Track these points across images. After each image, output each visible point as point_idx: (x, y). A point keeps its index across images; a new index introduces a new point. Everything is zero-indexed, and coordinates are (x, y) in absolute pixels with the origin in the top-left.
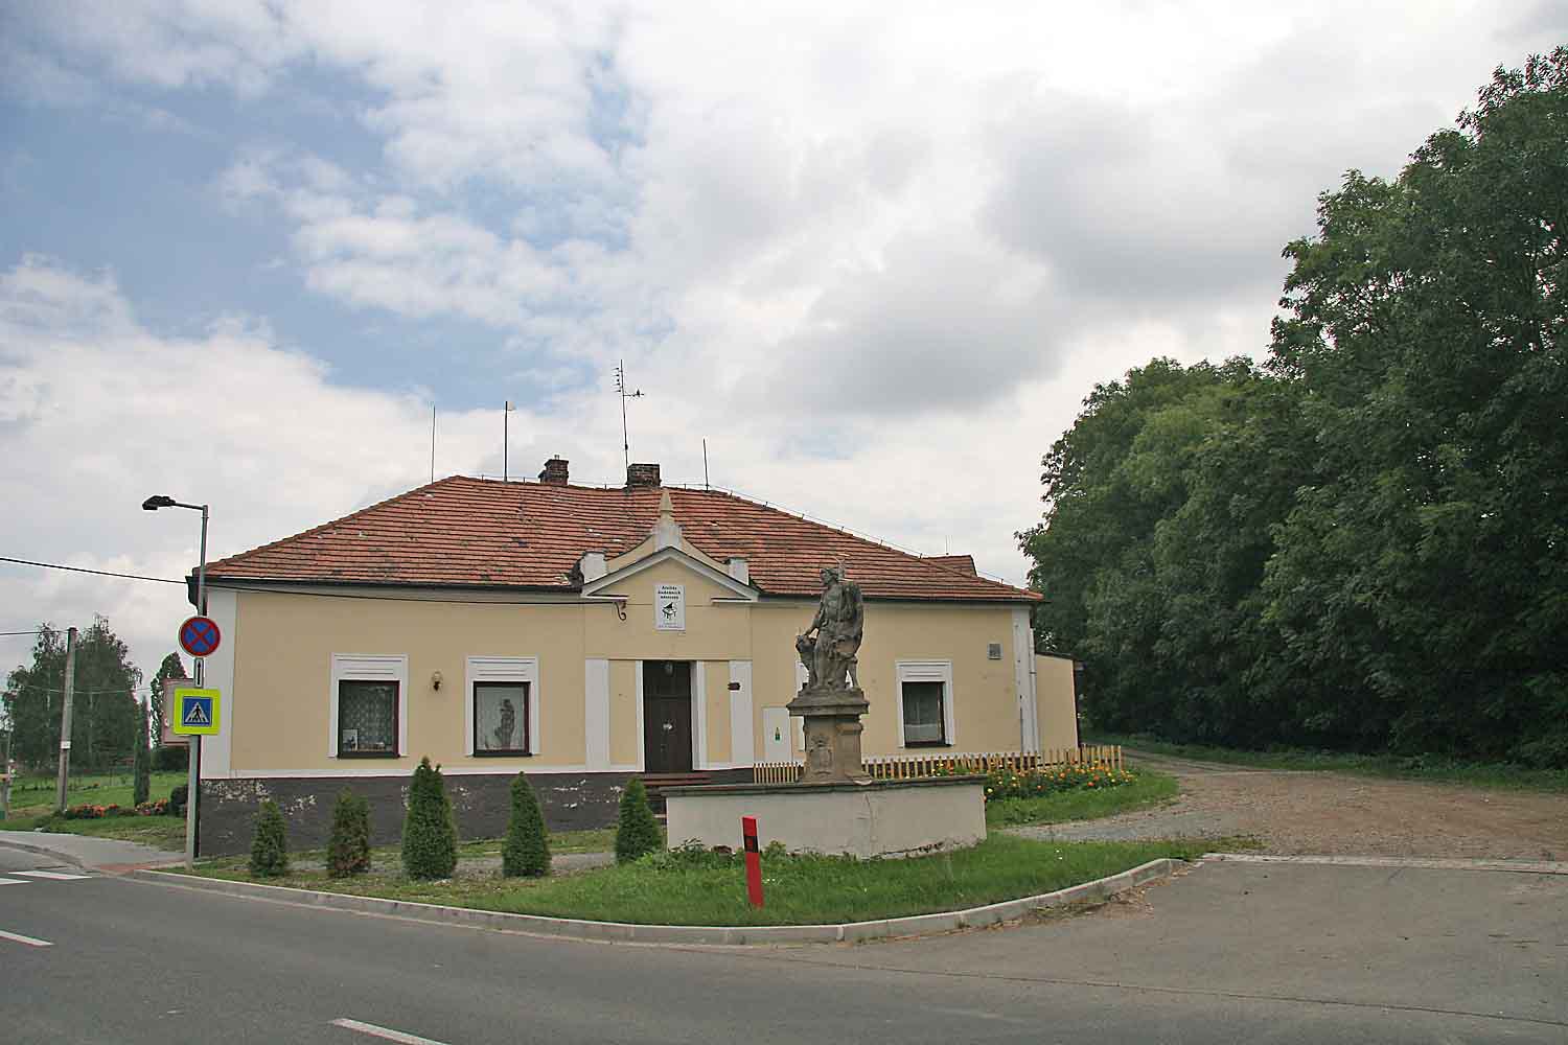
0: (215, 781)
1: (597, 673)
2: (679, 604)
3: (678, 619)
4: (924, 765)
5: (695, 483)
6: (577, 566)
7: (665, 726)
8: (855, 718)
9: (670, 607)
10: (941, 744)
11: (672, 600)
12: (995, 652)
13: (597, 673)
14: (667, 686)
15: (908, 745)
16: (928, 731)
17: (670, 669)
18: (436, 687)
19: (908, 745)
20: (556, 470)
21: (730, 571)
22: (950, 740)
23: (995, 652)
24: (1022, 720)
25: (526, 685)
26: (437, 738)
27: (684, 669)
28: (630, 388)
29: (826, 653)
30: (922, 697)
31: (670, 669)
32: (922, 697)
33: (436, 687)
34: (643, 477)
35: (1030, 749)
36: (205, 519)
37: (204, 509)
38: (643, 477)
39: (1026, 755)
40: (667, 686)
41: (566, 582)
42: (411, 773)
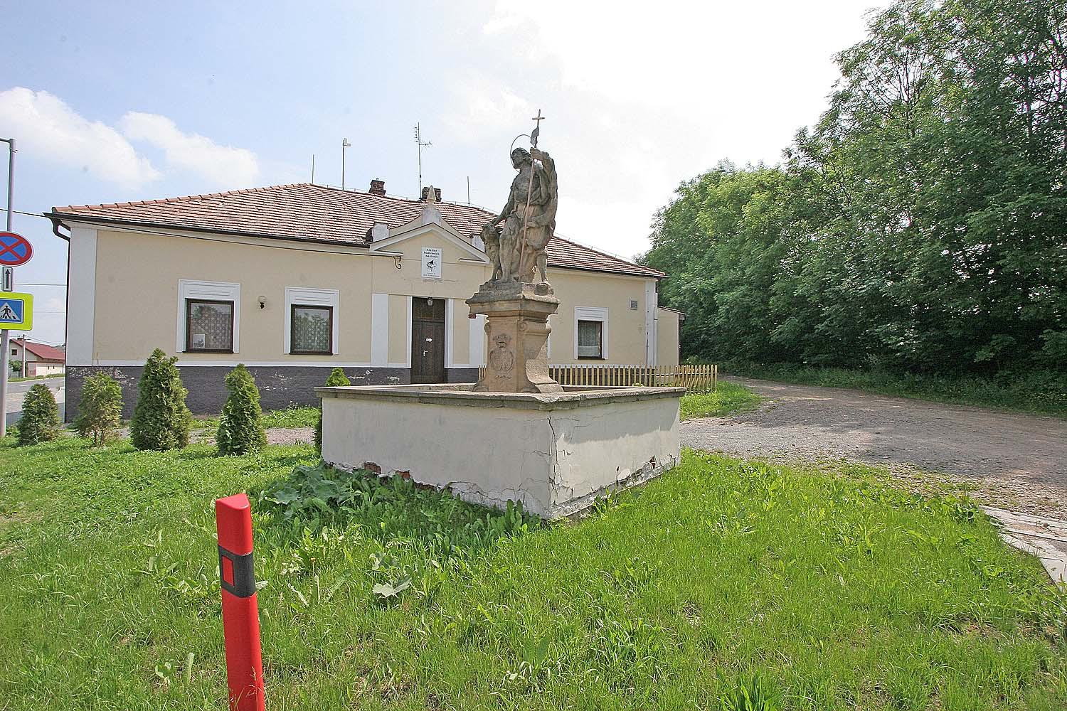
0: (79, 368)
1: (380, 303)
2: (438, 261)
3: (437, 271)
4: (587, 371)
5: (462, 201)
6: (370, 231)
7: (427, 340)
8: (541, 319)
9: (432, 262)
10: (600, 358)
11: (434, 258)
12: (634, 305)
13: (380, 303)
14: (429, 314)
15: (580, 358)
16: (592, 350)
17: (430, 303)
18: (262, 307)
19: (580, 358)
20: (378, 187)
21: (473, 242)
22: (605, 355)
23: (634, 305)
24: (647, 346)
25: (330, 308)
26: (261, 345)
27: (441, 303)
28: (424, 139)
29: (513, 244)
30: (589, 328)
31: (430, 303)
32: (589, 328)
33: (262, 307)
34: (430, 195)
35: (651, 365)
36: (12, 151)
37: (11, 141)
38: (430, 195)
39: (648, 368)
40: (429, 314)
41: (363, 241)
42: (143, 363)
